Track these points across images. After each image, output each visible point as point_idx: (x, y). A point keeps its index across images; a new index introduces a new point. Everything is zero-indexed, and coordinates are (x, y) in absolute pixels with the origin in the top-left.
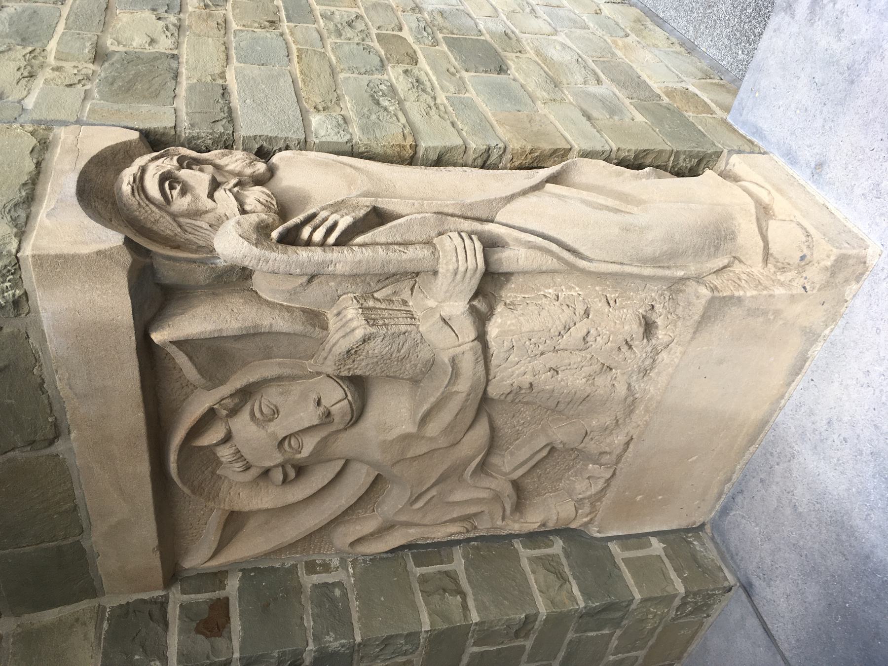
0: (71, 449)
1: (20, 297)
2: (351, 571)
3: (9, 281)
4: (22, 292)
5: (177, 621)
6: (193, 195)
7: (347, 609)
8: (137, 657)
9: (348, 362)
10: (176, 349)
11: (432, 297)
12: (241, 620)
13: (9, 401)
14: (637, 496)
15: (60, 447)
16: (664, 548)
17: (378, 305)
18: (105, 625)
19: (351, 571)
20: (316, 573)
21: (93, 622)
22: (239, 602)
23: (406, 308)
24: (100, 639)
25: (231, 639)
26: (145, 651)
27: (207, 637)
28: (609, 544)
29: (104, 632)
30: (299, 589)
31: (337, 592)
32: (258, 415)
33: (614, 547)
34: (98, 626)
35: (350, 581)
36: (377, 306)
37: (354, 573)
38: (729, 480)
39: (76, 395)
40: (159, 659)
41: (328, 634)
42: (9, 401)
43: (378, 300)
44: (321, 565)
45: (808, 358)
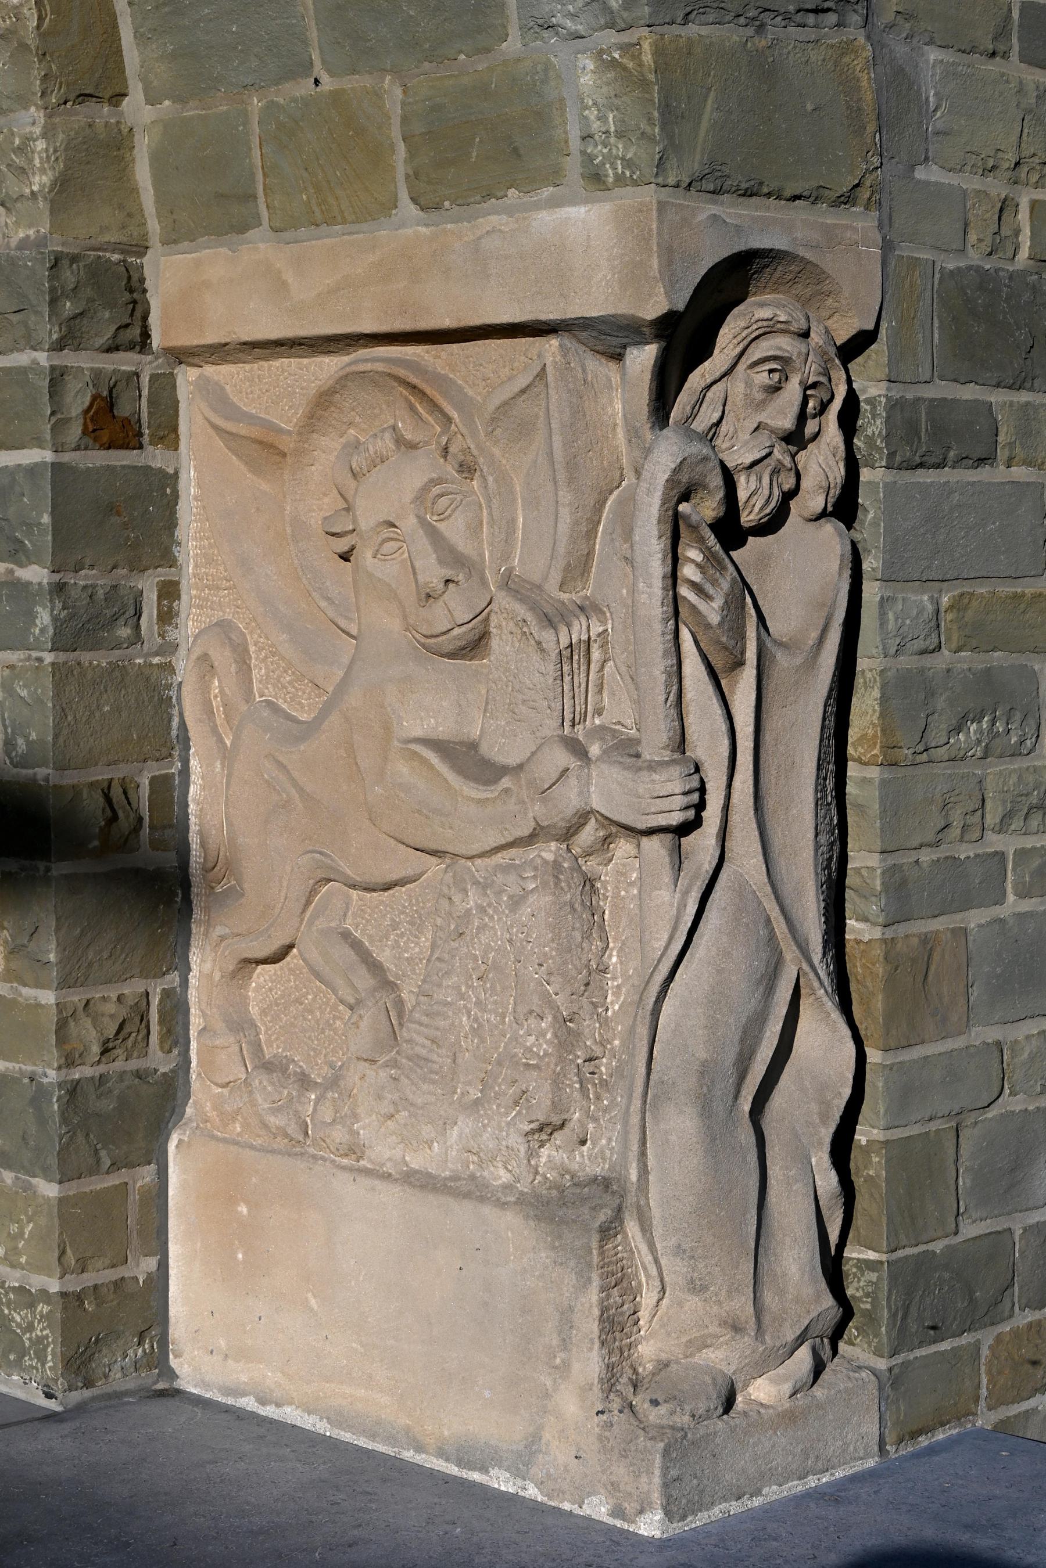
0: (403, 225)
1: (604, 182)
2: (156, 660)
3: (623, 172)
4: (610, 186)
5: (112, 367)
6: (763, 402)
7: (95, 647)
8: (68, 304)
9: (511, 624)
10: (535, 373)
11: (604, 752)
12: (102, 467)
13: (474, 154)
14: (247, 1203)
15: (408, 208)
16: (136, 1279)
17: (594, 667)
18: (116, 257)
19: (156, 660)
20: (159, 597)
21: (125, 239)
22: (129, 467)
23: (589, 715)
24: (99, 249)
25: (77, 448)
26: (74, 318)
27: (86, 412)
28: (153, 1167)
29: (108, 255)
30: (138, 567)
31: (124, 632)
32: (436, 490)
33: (146, 1175)
34: (116, 247)
35: (139, 657)
36: (592, 666)
37: (151, 665)
38: (263, 1402)
39: (479, 238)
40: (61, 339)
41: (64, 608)
42: (474, 154)
43: (602, 668)
44: (170, 608)
45: (487, 1472)
